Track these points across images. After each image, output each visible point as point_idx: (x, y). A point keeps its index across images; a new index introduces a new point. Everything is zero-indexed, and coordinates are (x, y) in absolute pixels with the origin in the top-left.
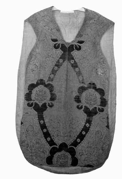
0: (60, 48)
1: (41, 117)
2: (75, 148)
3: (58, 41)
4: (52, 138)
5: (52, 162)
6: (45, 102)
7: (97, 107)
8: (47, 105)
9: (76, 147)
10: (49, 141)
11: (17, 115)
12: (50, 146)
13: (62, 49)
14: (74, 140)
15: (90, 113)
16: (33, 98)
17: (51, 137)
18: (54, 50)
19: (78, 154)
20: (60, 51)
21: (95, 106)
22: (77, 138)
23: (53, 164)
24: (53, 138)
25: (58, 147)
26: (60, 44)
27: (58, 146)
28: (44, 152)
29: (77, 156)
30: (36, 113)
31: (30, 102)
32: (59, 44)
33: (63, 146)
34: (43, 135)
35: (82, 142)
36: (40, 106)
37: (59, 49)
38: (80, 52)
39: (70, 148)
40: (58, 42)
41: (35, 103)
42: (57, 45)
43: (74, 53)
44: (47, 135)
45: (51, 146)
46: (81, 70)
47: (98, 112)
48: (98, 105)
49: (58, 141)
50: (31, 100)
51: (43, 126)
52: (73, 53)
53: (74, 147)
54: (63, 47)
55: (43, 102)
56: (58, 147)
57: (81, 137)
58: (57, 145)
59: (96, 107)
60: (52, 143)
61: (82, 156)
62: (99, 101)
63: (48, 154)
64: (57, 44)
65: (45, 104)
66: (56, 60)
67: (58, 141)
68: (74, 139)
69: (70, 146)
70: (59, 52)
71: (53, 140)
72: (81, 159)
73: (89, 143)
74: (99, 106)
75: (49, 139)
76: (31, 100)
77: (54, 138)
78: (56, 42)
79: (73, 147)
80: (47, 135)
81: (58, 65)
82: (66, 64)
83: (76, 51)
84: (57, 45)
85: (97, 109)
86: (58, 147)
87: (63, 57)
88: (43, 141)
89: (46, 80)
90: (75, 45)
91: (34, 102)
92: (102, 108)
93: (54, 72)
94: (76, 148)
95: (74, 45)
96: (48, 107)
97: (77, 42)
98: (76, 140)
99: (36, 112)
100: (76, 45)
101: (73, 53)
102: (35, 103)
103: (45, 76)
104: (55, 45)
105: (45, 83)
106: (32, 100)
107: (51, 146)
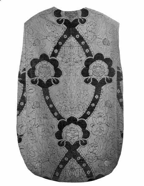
2: (85, 120)
5: (61, 16)
7: (105, 77)
10: (56, 115)
11: (18, 94)
17: (57, 112)
18: (59, 147)
19: (89, 126)
21: (103, 77)
22: (85, 51)
24: (61, 113)
25: (66, 120)
26: (65, 142)
27: (66, 119)
29: (89, 128)
30: (41, 88)
34: (50, 110)
36: (45, 83)
37: (63, 146)
41: (39, 79)
43: (79, 28)
44: (53, 110)
45: (58, 120)
48: (105, 76)
53: (84, 119)
56: (66, 121)
57: (91, 109)
58: (65, 119)
60: (59, 117)
61: (93, 126)
62: (107, 71)
67: (66, 116)
70: (64, 150)
72: (94, 166)
75: (56, 114)
77: (61, 112)
80: (53, 110)
82: (72, 40)
84: (61, 143)
85: (105, 81)
86: (66, 120)
89: (49, 53)
91: (38, 78)
93: (58, 47)
94: (87, 119)
96: (53, 83)
97: (82, 138)
98: (87, 174)
99: (40, 87)
100: (81, 19)
102: (39, 79)
104: (59, 142)
106: (36, 76)
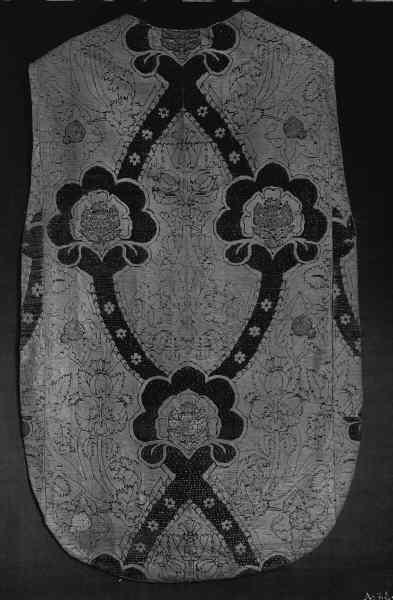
1: (105, 291)
2: (230, 382)
7: (293, 241)
8: (124, 255)
9: (231, 377)
13: (169, 463)
14: (224, 358)
16: (76, 233)
23: (150, 48)
24: (152, 356)
29: (240, 408)
31: (65, 246)
32: (162, 446)
35: (253, 359)
38: (232, 465)
42: (145, 60)
44: (128, 346)
50: (70, 239)
51: (114, 321)
54: (174, 460)
55: (112, 245)
60: (146, 369)
63: (137, 408)
64: (148, 57)
65: (118, 250)
66: (145, 110)
67: (170, 367)
68: (224, 355)
69: (211, 375)
74: (299, 240)
76: (70, 239)
78: (151, 443)
79: (223, 377)
81: (155, 123)
84: (145, 60)
88: (118, 363)
89: (112, 167)
95: (205, 56)
101: (209, 477)
107: (145, 378)
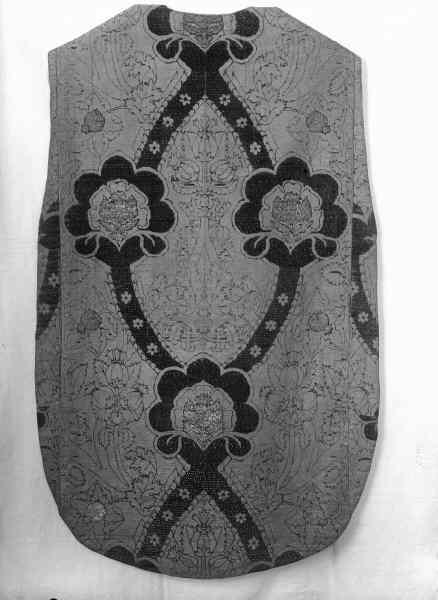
0: (179, 450)
3: (172, 32)
4: (163, 344)
6: (134, 235)
7: (311, 237)
9: (246, 370)
12: (157, 370)
13: (185, 454)
15: (290, 262)
20: (179, 460)
25: (184, 371)
27: (186, 368)
28: (141, 388)
33: (204, 370)
38: (248, 459)
39: (226, 375)
40: (171, 36)
43: (228, 470)
46: (255, 123)
47: (318, 256)
49: (185, 355)
52: (225, 72)
58: (180, 366)
59: (305, 224)
60: (162, 359)
63: (152, 398)
67: (185, 355)
69: (225, 368)
71: (168, 350)
73: (288, 353)
83: (234, 457)
84: (168, 441)
86: (184, 371)
87: (192, 88)
90: (233, 43)
92: (328, 241)
93: (160, 134)
100: (234, 441)
101: (225, 72)
102: (102, 239)
103: (129, 145)
105: (130, 170)
